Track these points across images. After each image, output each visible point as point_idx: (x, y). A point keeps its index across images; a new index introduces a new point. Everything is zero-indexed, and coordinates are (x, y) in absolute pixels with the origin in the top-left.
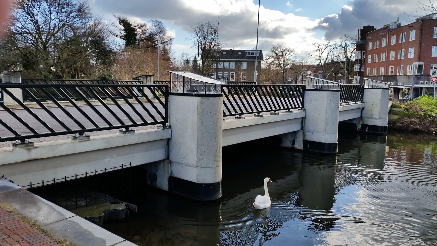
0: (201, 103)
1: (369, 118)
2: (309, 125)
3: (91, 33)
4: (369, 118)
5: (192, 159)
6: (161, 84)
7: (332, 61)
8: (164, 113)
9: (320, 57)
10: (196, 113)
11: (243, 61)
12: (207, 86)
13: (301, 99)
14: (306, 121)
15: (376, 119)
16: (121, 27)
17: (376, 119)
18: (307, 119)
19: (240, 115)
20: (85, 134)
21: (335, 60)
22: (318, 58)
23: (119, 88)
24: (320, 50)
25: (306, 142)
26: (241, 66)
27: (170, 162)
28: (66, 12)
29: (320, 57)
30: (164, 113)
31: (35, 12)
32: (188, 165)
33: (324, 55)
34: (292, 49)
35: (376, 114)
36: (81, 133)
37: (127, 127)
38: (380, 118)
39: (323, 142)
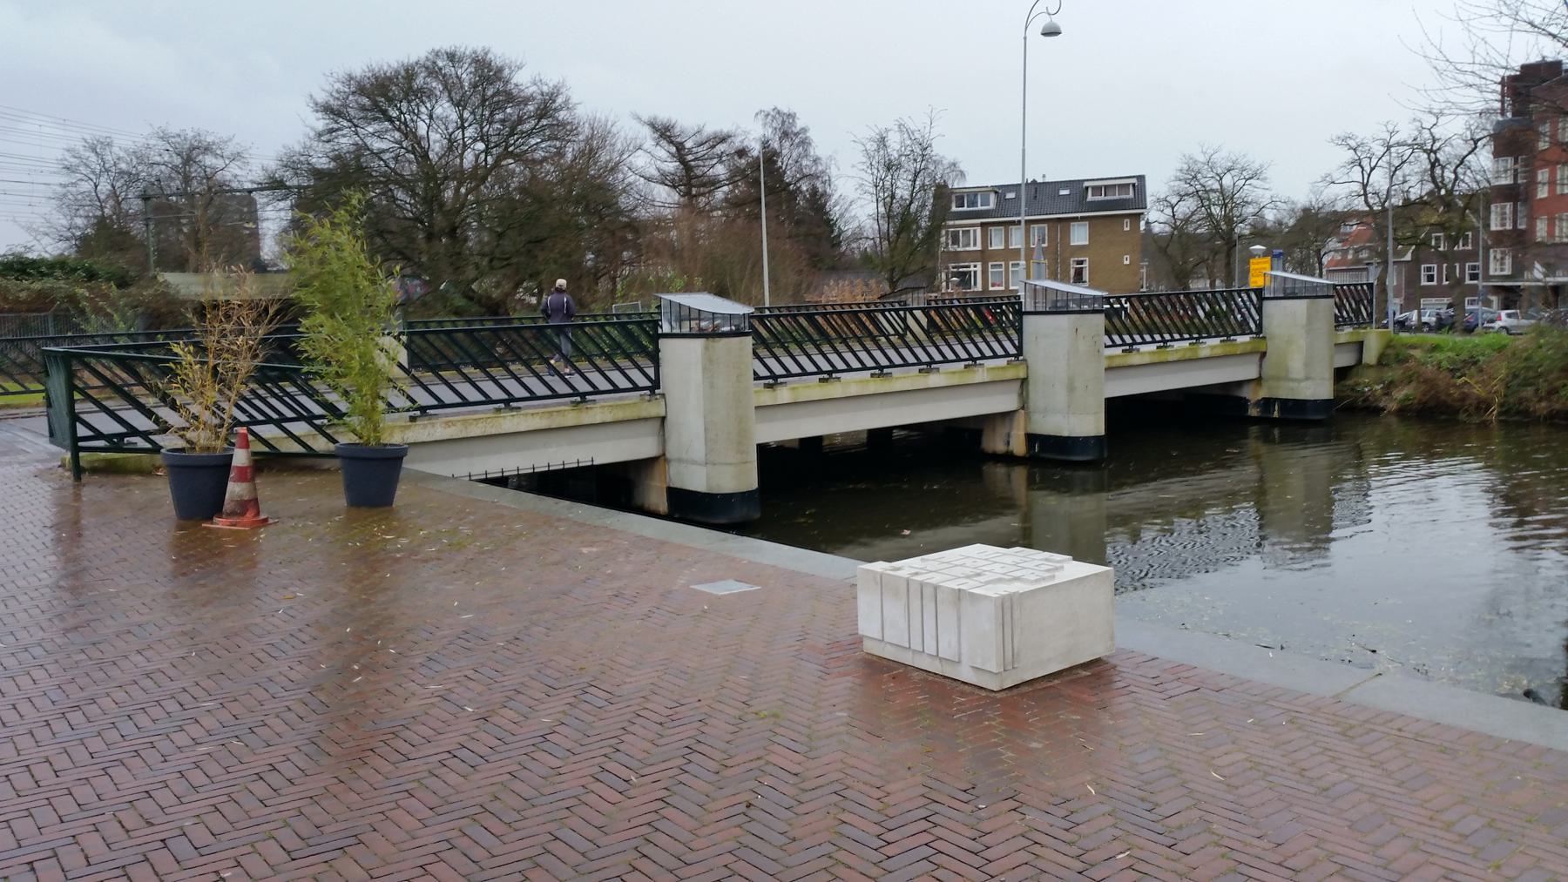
0: (706, 348)
1: (1279, 379)
2: (1036, 397)
3: (571, 175)
4: (1279, 379)
5: (698, 451)
6: (830, 309)
7: (1407, 200)
8: (652, 374)
9: (1365, 186)
10: (700, 367)
11: (1075, 219)
12: (1082, 299)
13: (1015, 337)
14: (1031, 387)
15: (1299, 381)
16: (663, 152)
17: (1299, 381)
18: (1031, 381)
19: (829, 373)
20: (513, 404)
21: (1413, 197)
22: (1357, 187)
23: (431, 338)
24: (1365, 163)
25: (1031, 438)
26: (1066, 235)
27: (666, 460)
28: (503, 121)
29: (1365, 186)
30: (652, 374)
31: (422, 129)
32: (694, 462)
33: (1379, 180)
34: (1256, 165)
35: (1296, 365)
36: (506, 402)
37: (583, 395)
38: (1307, 378)
39: (1066, 434)
